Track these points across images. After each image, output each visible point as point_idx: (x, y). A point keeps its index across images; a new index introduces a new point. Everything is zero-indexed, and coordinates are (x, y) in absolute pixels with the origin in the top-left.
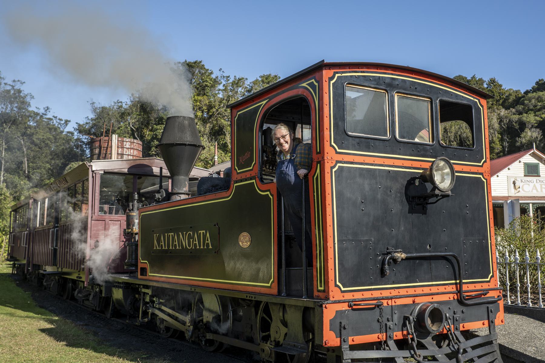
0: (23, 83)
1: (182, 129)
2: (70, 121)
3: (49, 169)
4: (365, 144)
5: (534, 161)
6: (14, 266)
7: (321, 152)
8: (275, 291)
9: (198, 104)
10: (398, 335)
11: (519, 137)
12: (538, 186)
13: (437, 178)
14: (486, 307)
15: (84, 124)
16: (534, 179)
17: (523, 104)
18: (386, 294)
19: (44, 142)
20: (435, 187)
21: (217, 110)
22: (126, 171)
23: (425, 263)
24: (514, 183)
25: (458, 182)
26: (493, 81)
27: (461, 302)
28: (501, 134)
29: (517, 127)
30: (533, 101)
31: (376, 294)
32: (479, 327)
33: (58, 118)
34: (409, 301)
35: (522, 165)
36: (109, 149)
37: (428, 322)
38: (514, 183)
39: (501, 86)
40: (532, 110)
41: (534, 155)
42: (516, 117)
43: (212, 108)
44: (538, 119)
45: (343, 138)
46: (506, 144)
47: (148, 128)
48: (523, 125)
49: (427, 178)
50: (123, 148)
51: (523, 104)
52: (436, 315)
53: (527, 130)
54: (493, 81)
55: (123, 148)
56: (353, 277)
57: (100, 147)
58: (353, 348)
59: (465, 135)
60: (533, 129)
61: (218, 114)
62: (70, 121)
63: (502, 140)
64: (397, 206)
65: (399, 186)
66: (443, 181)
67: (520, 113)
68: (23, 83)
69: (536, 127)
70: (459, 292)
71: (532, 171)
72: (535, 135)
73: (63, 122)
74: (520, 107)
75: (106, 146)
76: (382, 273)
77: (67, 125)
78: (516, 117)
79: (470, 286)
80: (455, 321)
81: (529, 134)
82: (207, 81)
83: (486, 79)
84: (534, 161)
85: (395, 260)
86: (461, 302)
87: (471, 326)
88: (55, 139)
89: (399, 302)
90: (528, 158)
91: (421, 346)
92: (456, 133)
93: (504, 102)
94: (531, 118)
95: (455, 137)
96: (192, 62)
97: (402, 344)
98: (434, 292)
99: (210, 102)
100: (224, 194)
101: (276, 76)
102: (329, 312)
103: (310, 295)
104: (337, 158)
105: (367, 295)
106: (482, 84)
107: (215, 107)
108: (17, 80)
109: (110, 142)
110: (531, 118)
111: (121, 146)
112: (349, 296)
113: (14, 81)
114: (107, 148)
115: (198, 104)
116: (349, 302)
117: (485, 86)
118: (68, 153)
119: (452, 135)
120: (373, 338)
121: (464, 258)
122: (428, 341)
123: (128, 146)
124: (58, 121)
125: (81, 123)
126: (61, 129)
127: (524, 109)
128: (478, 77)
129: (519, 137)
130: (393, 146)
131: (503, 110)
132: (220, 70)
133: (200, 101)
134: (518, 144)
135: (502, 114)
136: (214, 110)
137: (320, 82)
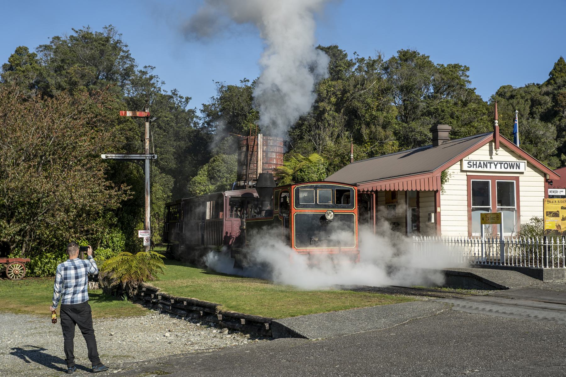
0: (153, 68)
2: (190, 98)
3: (175, 153)
6: (204, 263)
9: (332, 89)
15: (210, 105)
19: (168, 124)
21: (352, 95)
33: (178, 96)
36: (255, 147)
43: (346, 93)
50: (267, 145)
61: (353, 98)
62: (190, 98)
68: (153, 68)
73: (183, 100)
75: (252, 144)
77: (187, 103)
82: (340, 66)
88: (177, 118)
96: (326, 47)
99: (344, 86)
101: (415, 52)
107: (349, 91)
108: (147, 65)
109: (256, 140)
113: (146, 67)
114: (254, 146)
115: (332, 89)
116: (543, 220)
118: (194, 136)
123: (271, 144)
124: (179, 99)
125: (207, 104)
126: (182, 108)
132: (355, 53)
133: (334, 86)
136: (349, 94)
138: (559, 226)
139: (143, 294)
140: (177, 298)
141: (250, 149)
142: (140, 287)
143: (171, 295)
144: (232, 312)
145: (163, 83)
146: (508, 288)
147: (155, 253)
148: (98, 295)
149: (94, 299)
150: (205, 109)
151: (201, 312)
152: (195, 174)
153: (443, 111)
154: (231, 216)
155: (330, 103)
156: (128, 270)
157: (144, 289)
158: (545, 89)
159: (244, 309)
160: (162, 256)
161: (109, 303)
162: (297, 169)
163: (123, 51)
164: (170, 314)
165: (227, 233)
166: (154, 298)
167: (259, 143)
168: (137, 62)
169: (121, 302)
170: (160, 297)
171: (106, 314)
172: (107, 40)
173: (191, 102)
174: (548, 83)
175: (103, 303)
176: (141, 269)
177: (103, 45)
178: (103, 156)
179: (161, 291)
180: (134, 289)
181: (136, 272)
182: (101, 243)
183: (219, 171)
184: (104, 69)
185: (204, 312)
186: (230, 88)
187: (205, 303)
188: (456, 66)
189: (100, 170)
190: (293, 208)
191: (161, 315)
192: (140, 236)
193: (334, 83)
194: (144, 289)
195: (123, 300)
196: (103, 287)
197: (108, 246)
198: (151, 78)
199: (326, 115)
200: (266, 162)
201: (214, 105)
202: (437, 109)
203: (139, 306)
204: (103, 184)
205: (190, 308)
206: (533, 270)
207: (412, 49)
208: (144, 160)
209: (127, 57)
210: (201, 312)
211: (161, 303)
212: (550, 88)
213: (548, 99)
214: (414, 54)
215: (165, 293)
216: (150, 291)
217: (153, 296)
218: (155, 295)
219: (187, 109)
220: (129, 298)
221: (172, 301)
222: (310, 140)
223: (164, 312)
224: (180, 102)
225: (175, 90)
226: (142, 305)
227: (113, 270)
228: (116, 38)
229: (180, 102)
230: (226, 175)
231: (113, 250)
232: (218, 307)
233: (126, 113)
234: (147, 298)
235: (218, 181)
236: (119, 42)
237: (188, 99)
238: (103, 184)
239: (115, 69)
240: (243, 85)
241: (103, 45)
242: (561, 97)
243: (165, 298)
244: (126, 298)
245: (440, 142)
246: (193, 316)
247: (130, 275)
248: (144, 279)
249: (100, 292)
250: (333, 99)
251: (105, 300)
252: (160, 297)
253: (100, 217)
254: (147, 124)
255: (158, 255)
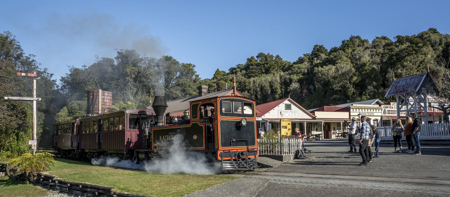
1: (161, 100)
4: (226, 115)
5: (289, 103)
7: (217, 117)
8: (205, 149)
10: (234, 158)
11: (289, 86)
12: (290, 114)
13: (243, 123)
14: (253, 152)
16: (289, 111)
17: (291, 70)
18: (231, 149)
20: (242, 124)
22: (137, 113)
23: (240, 142)
24: (281, 113)
25: (248, 123)
26: (278, 57)
27: (248, 151)
28: (281, 84)
29: (289, 81)
30: (296, 69)
31: (229, 149)
32: (252, 157)
34: (236, 151)
35: (284, 105)
37: (240, 155)
38: (281, 113)
39: (282, 59)
40: (295, 73)
41: (289, 100)
42: (288, 77)
44: (298, 78)
45: (222, 114)
46: (283, 90)
47: (104, 82)
48: (291, 81)
49: (240, 122)
50: (104, 96)
51: (291, 70)
52: (242, 154)
53: (293, 83)
54: (278, 57)
55: (104, 96)
56: (223, 145)
57: (93, 96)
58: (224, 160)
59: (263, 85)
60: (296, 83)
63: (281, 88)
64: (234, 129)
65: (234, 124)
66: (244, 123)
67: (290, 75)
69: (297, 82)
70: (248, 149)
71: (288, 107)
72: (296, 86)
74: (290, 71)
76: (230, 144)
78: (288, 77)
79: (250, 147)
80: (247, 156)
81: (294, 85)
83: (275, 55)
84: (289, 103)
85: (233, 141)
86: (248, 151)
87: (250, 157)
88: (46, 84)
89: (234, 151)
90: (286, 102)
91: (239, 161)
92: (259, 84)
93: (283, 67)
94: (295, 77)
95: (259, 85)
97: (235, 160)
98: (242, 148)
100: (188, 125)
102: (219, 152)
103: (214, 149)
104: (220, 118)
105: (227, 149)
106: (273, 58)
110: (295, 77)
111: (103, 95)
112: (223, 149)
113: (30, 55)
117: (274, 59)
119: (257, 85)
120: (228, 158)
121: (249, 141)
122: (240, 160)
125: (64, 77)
127: (292, 72)
128: (271, 54)
129: (289, 86)
130: (233, 115)
131: (282, 72)
133: (134, 70)
134: (289, 90)
135: (282, 74)
137: (217, 101)
138: (287, 133)
139: (41, 180)
140: (72, 183)
141: (95, 97)
142: (39, 175)
143: (67, 181)
144: (126, 193)
145: (40, 64)
146: (272, 167)
147: (48, 153)
148: (6, 181)
149: (3, 184)
150: (63, 79)
151: (96, 193)
152: (59, 111)
153: (185, 84)
154: (130, 128)
155: (131, 77)
156: (30, 165)
157: (42, 177)
158: (213, 81)
159: (133, 191)
160: (53, 155)
161: (16, 186)
162: (121, 108)
163: (16, 45)
164: (67, 193)
165: (128, 139)
166: (52, 182)
167: (100, 94)
168: (25, 51)
169: (25, 185)
170: (57, 182)
171: (16, 195)
172: (7, 38)
173: (53, 76)
174: (213, 79)
175: (11, 186)
176: (39, 164)
177: (4, 40)
178: (6, 98)
179: (57, 178)
180: (34, 176)
181: (36, 166)
182: (4, 148)
183: (75, 109)
184: (4, 54)
185: (98, 192)
186: (76, 70)
187: (98, 186)
188: (190, 65)
189: (4, 106)
190: (218, 116)
191: (60, 194)
192: (30, 144)
193: (134, 68)
194: (42, 177)
195: (26, 184)
196: (9, 175)
197: (8, 150)
198: (33, 61)
199: (129, 83)
200: (104, 103)
201: (67, 77)
202: (183, 83)
203: (39, 187)
204: (6, 113)
205: (85, 189)
206: (277, 156)
207: (169, 56)
208: (32, 101)
209: (19, 48)
210: (96, 193)
211: (58, 186)
212: (215, 80)
213: (215, 84)
214: (171, 58)
215: (61, 179)
216: (47, 178)
217: (50, 181)
218: (52, 180)
219: (52, 79)
220: (30, 182)
221: (69, 185)
222: (121, 96)
223: (61, 192)
224: (48, 76)
225: (46, 69)
226: (41, 186)
227: (19, 165)
228: (12, 38)
229: (48, 76)
230: (78, 111)
231: (12, 152)
232: (113, 190)
233: (21, 74)
234: (45, 182)
235: (74, 114)
236: (14, 40)
237: (52, 75)
238: (6, 113)
239: (11, 54)
240: (83, 68)
241: (4, 40)
242: (220, 84)
243: (60, 182)
244: (28, 182)
245: (203, 94)
246: (87, 195)
247: (32, 167)
248: (42, 170)
249: (7, 178)
250: (133, 76)
251: (12, 184)
252: (57, 182)
253: (3, 133)
254: (35, 81)
255: (50, 154)
